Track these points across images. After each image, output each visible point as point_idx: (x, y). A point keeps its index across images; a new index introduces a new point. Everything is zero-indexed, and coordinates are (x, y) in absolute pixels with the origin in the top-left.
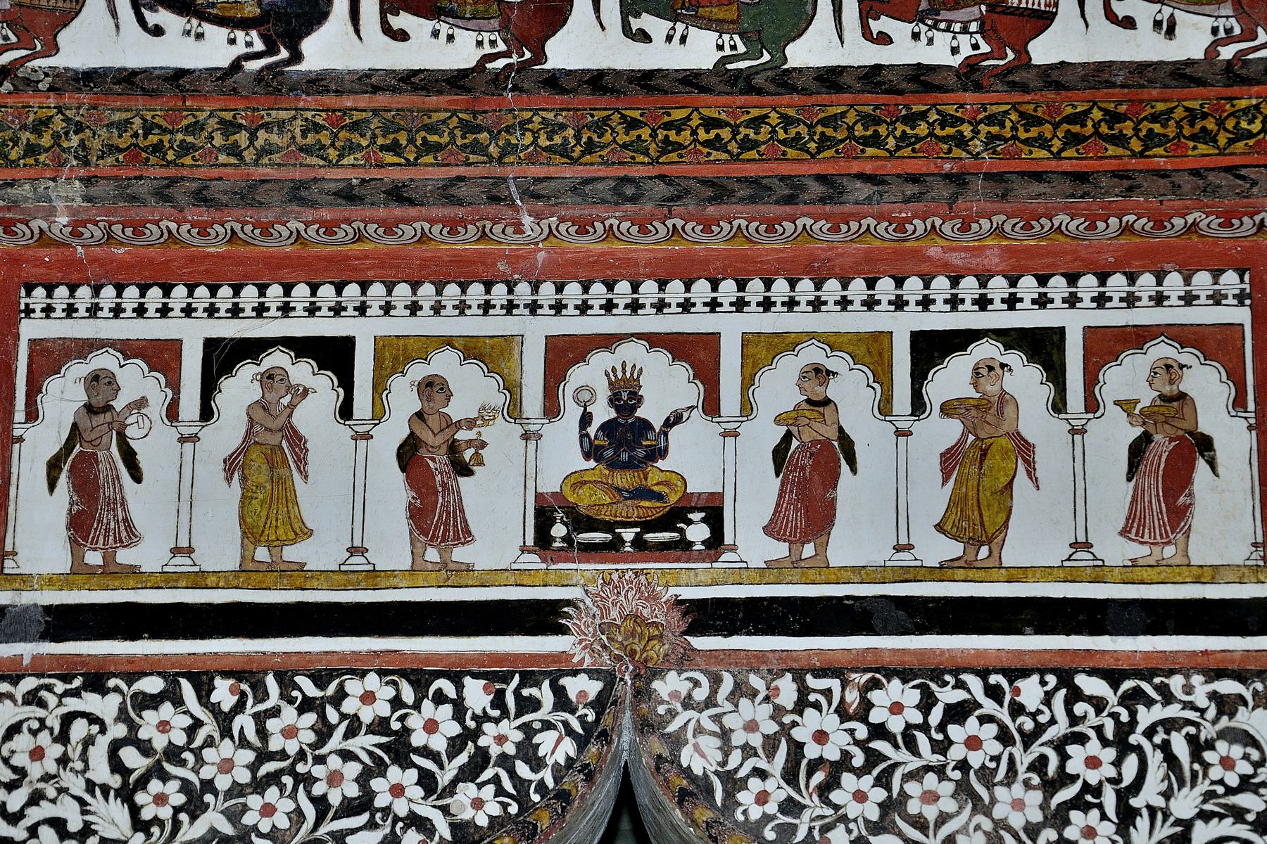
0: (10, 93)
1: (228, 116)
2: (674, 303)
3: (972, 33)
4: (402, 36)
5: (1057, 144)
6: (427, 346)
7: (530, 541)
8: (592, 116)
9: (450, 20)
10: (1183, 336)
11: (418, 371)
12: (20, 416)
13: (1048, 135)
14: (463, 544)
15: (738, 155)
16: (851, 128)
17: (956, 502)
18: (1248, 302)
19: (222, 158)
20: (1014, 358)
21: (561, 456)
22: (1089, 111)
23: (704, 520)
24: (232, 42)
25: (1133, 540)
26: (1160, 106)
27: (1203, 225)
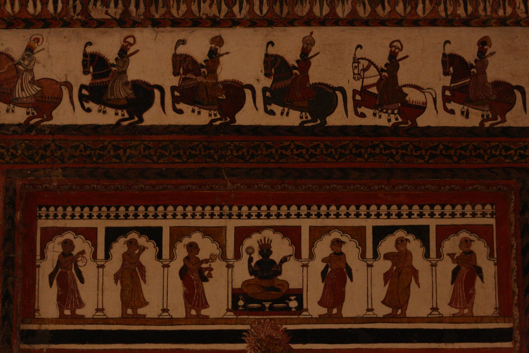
0: (35, 135)
1: (116, 143)
2: (283, 214)
3: (395, 114)
4: (180, 112)
5: (427, 158)
6: (189, 231)
7: (230, 307)
8: (253, 144)
9: (199, 106)
10: (471, 229)
11: (186, 241)
12: (38, 258)
13: (424, 154)
14: (205, 308)
15: (309, 160)
16: (351, 150)
17: (389, 293)
18: (494, 216)
19: (114, 160)
20: (410, 237)
21: (242, 274)
22: (439, 145)
23: (295, 299)
24: (117, 114)
25: (453, 307)
26: (464, 144)
27: (479, 188)
